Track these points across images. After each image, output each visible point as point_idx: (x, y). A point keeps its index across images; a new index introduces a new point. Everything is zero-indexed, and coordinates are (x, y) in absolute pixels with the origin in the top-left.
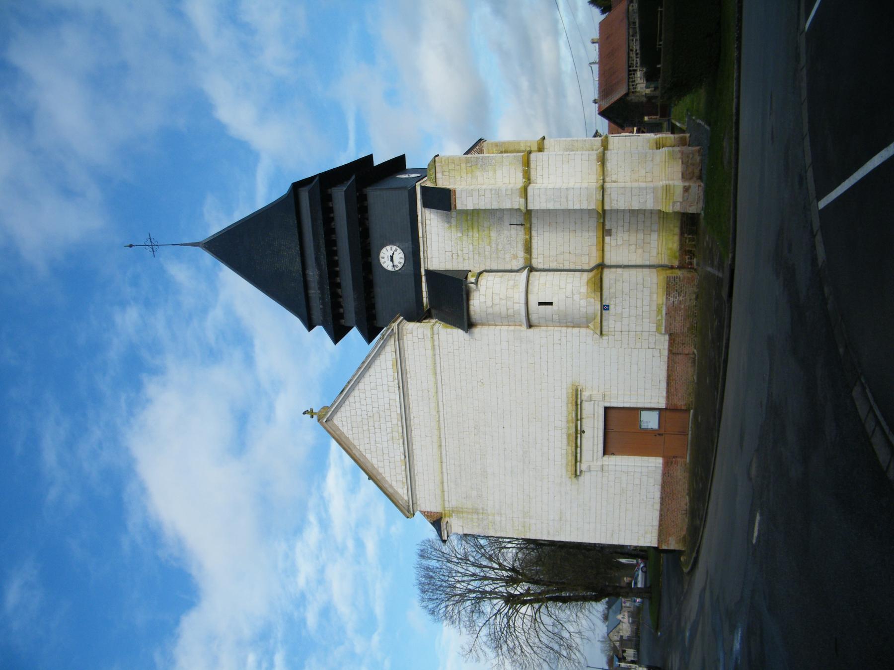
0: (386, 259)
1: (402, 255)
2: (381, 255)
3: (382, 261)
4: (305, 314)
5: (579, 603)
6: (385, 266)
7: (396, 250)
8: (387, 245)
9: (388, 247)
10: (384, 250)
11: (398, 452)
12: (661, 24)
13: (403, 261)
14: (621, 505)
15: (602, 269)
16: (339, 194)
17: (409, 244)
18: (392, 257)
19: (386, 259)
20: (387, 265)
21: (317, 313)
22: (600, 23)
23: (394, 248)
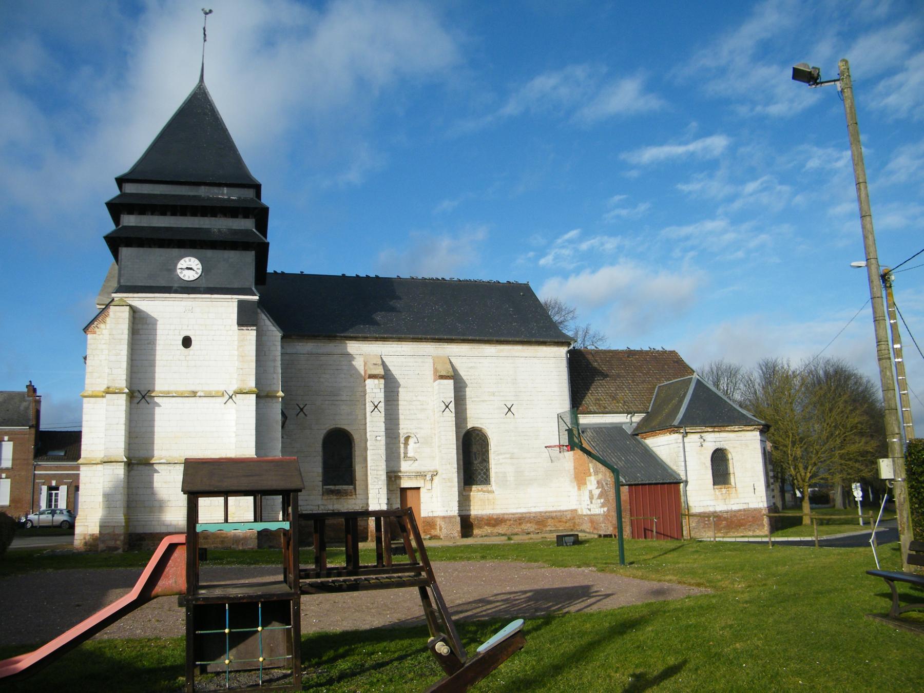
0: (188, 263)
1: (192, 278)
2: (193, 259)
3: (187, 259)
4: (129, 177)
5: (556, 318)
6: (182, 261)
7: (197, 273)
8: (200, 260)
9: (200, 266)
10: (197, 261)
11: (683, 468)
12: (243, 586)
13: (186, 278)
14: (155, 475)
15: (383, 377)
16: (248, 224)
17: (204, 284)
18: (191, 269)
19: (188, 263)
20: (184, 263)
21: (130, 188)
22: (673, 353)
23: (200, 272)
